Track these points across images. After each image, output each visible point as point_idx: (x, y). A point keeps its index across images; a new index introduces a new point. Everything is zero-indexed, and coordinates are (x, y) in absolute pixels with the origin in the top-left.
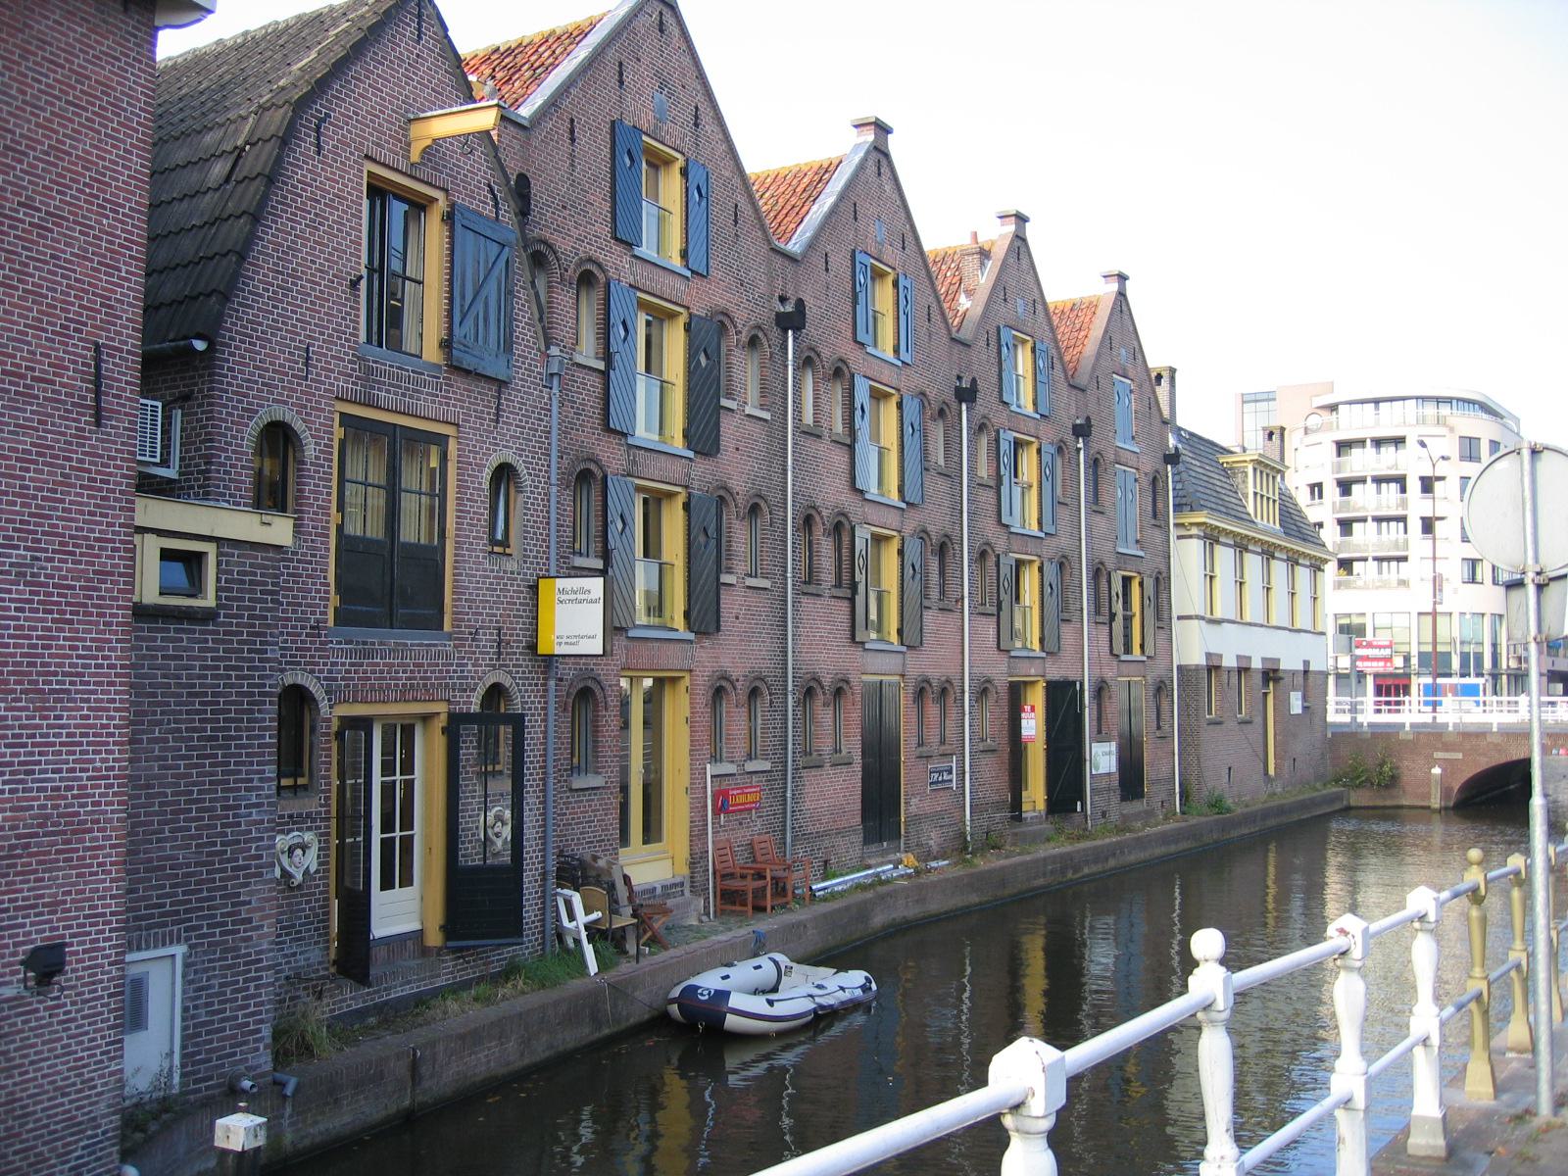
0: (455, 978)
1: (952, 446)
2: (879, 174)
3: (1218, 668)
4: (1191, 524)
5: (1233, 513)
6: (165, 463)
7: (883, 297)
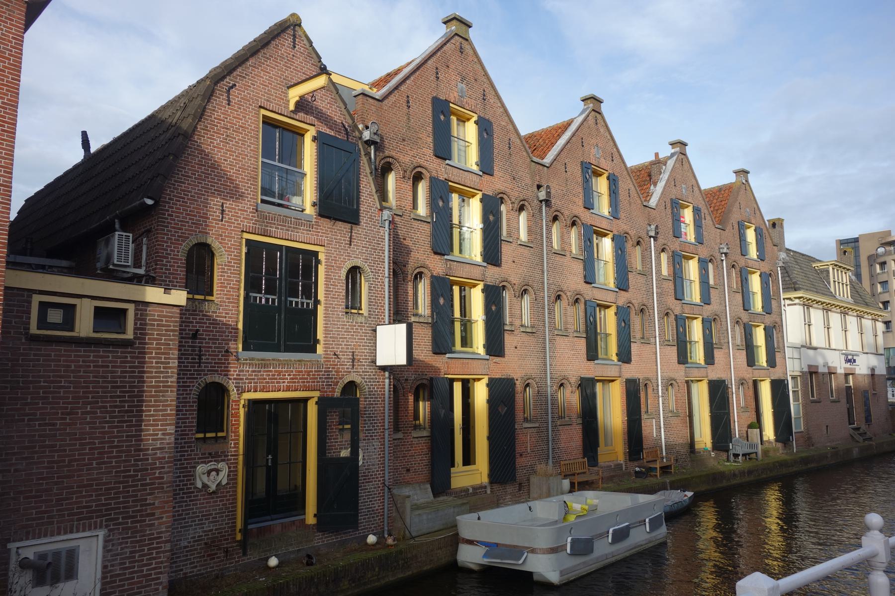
0: (324, 541)
1: (646, 259)
2: (596, 124)
3: (816, 373)
4: (795, 298)
6: (137, 264)
7: (602, 185)
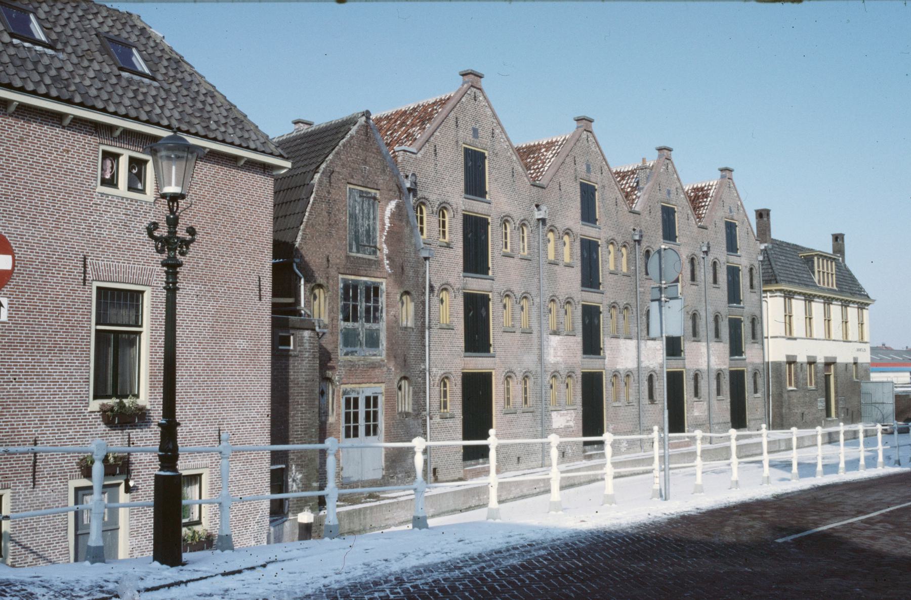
5: (803, 282)
